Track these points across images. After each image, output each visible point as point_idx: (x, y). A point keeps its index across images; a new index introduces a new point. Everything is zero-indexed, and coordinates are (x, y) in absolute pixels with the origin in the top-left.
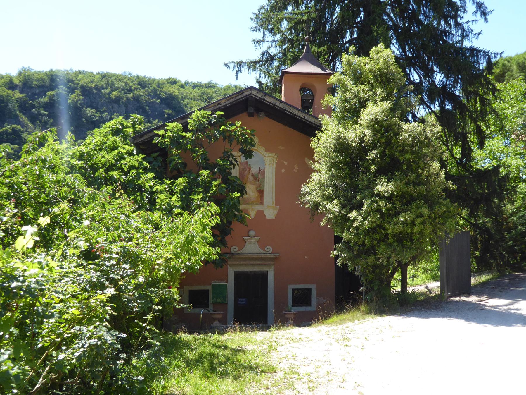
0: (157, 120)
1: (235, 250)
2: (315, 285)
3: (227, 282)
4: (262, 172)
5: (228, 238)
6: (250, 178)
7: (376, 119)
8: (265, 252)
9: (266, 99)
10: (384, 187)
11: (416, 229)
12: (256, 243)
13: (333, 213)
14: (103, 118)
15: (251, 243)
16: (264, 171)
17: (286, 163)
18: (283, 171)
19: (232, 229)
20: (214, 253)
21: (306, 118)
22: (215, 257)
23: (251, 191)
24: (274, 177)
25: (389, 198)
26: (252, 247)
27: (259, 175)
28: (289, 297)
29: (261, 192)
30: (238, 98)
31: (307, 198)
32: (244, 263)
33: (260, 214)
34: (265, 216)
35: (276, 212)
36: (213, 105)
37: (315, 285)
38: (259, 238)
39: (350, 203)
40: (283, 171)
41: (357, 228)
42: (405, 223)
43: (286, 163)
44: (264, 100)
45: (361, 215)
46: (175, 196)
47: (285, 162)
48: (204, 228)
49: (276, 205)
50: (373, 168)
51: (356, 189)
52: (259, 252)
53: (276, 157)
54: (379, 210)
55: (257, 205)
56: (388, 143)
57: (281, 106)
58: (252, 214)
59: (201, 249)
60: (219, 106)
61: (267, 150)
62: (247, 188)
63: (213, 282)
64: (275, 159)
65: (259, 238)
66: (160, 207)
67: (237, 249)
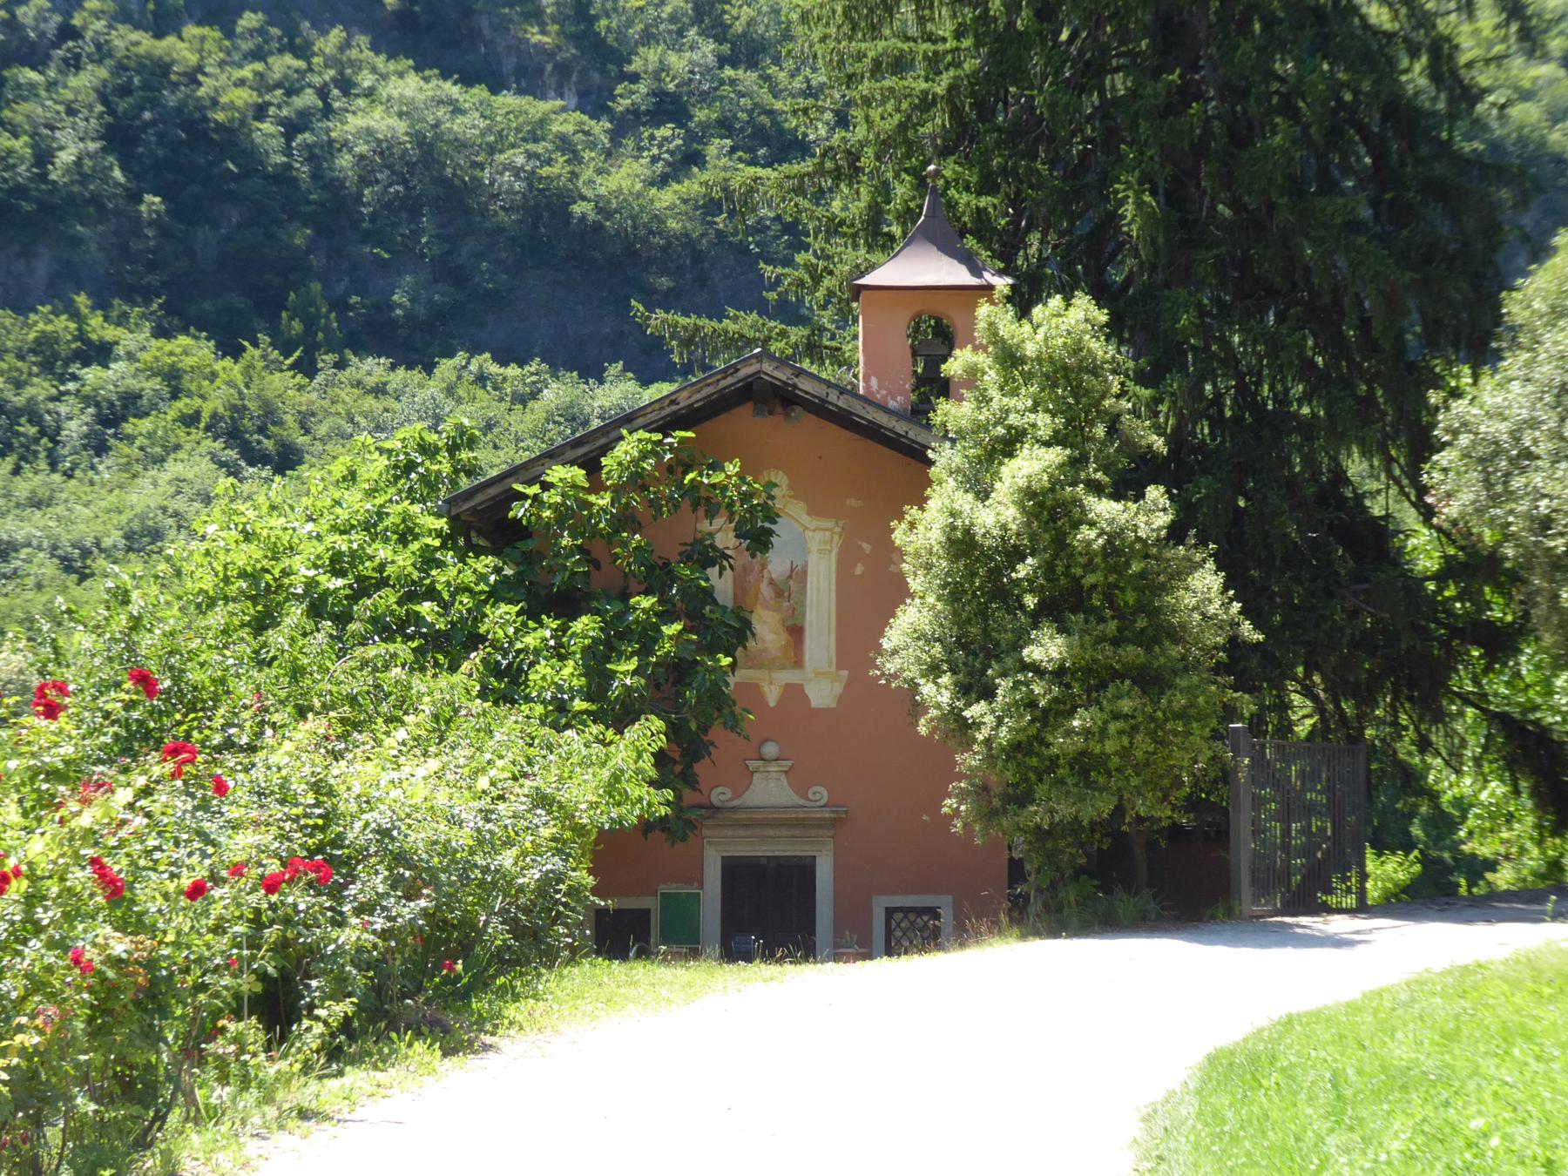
0: (336, 34)
1: (722, 797)
2: (949, 899)
3: (701, 886)
4: (799, 575)
5: (701, 768)
6: (766, 590)
7: (1029, 487)
8: (807, 803)
9: (800, 386)
10: (1047, 648)
11: (1110, 746)
12: (783, 777)
13: (938, 706)
14: (22, 27)
15: (767, 779)
16: (804, 572)
17: (867, 547)
18: (859, 569)
19: (712, 743)
20: (658, 802)
21: (911, 435)
22: (663, 811)
23: (767, 628)
24: (833, 588)
25: (1059, 673)
26: (770, 789)
27: (791, 582)
28: (875, 933)
29: (796, 632)
30: (723, 383)
31: (891, 666)
32: (748, 833)
33: (794, 694)
34: (808, 700)
35: (839, 688)
36: (657, 406)
37: (949, 899)
38: (789, 763)
39: (975, 688)
40: (859, 569)
41: (988, 742)
42: (1086, 732)
43: (867, 547)
44: (795, 386)
45: (993, 711)
46: (571, 663)
47: (865, 545)
48: (640, 756)
49: (839, 667)
50: (1030, 601)
51: (993, 652)
52: (790, 804)
53: (838, 530)
54: (1031, 704)
55: (783, 667)
56: (1060, 544)
57: (840, 404)
58: (772, 695)
59: (635, 792)
60: (674, 408)
61: (813, 511)
62: (754, 622)
63: (662, 889)
64: (836, 537)
65: (789, 763)
66: (539, 696)
67: (729, 796)
